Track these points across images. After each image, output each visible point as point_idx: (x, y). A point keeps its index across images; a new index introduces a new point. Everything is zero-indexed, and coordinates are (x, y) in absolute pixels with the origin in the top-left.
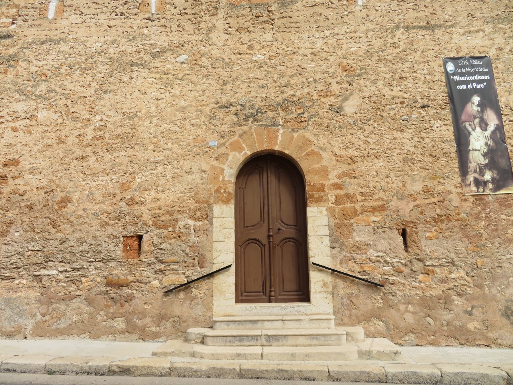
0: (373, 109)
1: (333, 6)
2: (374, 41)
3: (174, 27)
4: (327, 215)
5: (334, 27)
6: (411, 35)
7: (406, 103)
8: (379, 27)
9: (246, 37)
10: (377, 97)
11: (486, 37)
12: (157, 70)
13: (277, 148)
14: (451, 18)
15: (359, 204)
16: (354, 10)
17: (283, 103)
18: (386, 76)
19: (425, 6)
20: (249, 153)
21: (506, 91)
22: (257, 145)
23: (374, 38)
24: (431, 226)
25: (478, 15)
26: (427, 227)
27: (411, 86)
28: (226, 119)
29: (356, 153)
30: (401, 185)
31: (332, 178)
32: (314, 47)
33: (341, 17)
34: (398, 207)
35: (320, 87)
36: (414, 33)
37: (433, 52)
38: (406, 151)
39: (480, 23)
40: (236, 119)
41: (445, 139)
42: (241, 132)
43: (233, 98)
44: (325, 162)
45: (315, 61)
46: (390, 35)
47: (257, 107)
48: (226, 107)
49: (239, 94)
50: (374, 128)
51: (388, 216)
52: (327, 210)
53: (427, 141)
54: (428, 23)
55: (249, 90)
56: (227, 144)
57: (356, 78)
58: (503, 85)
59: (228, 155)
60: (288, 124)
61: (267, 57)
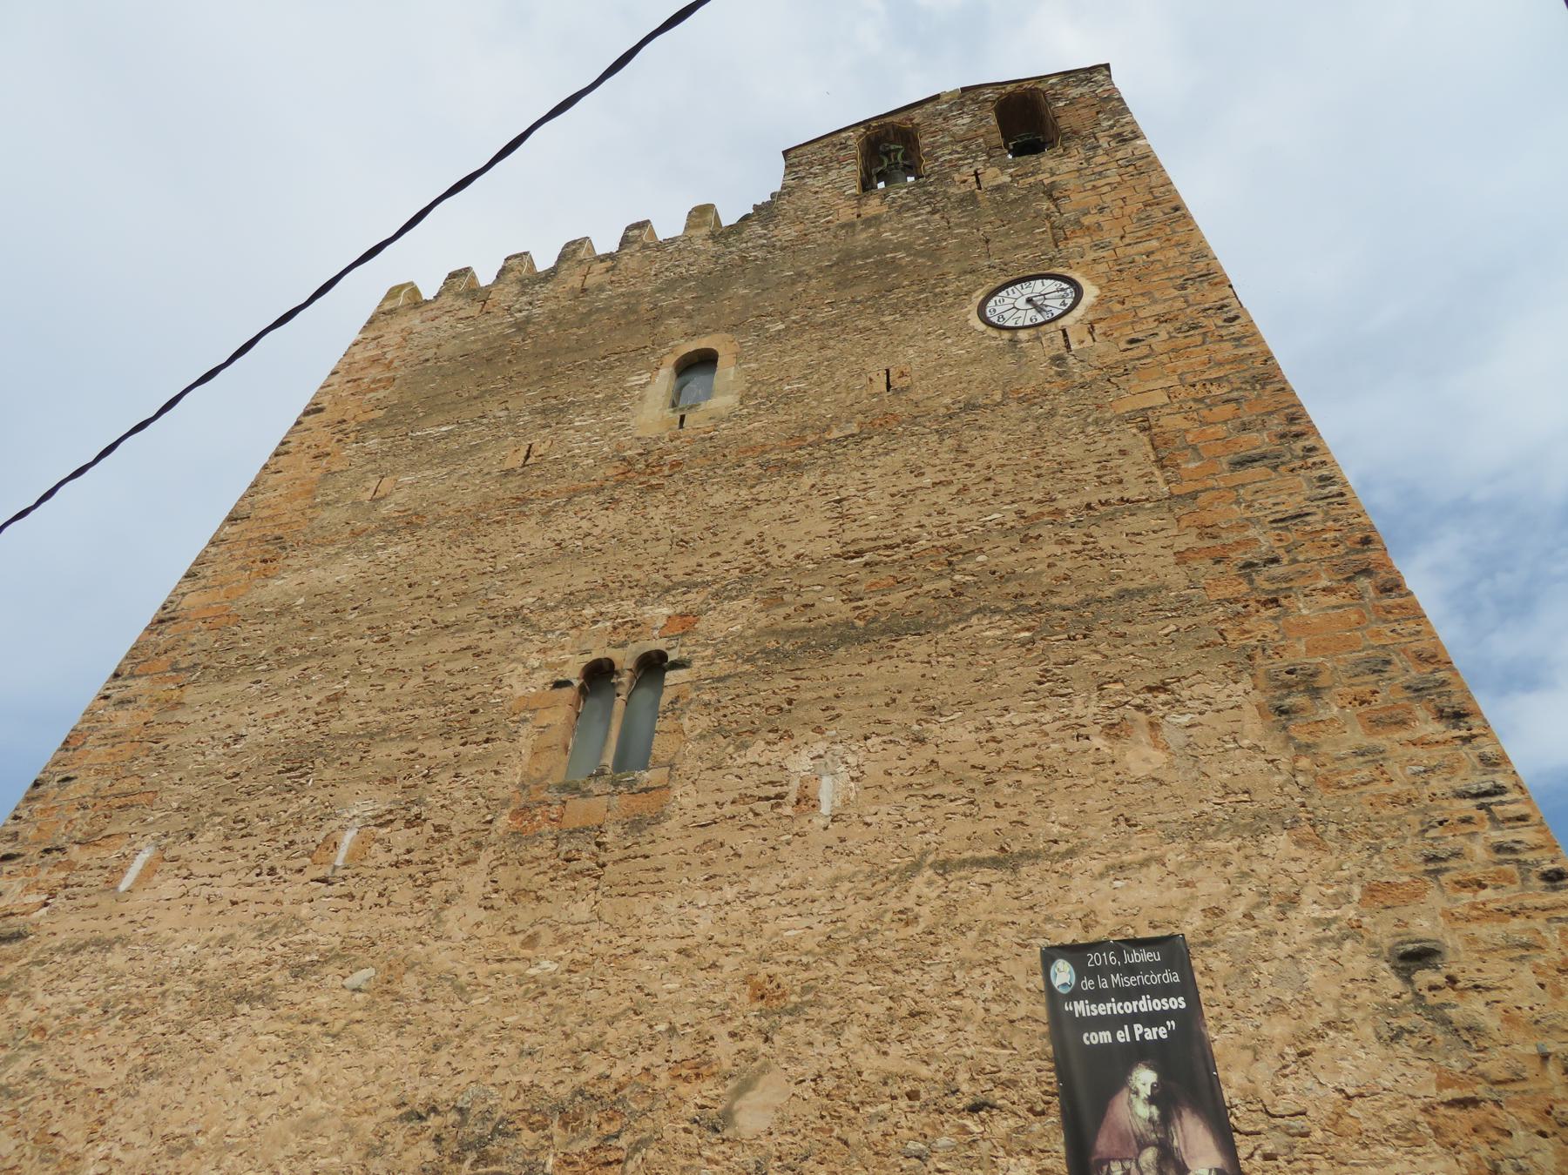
0: (822, 1117)
1: (758, 822)
2: (851, 908)
3: (372, 897)
6: (951, 886)
7: (924, 1096)
8: (866, 868)
9: (525, 914)
10: (839, 1077)
11: (1171, 879)
16: (807, 828)
19: (998, 805)
21: (1244, 1047)
23: (850, 900)
25: (1143, 817)
27: (942, 1038)
28: (406, 1156)
36: (961, 879)
37: (1013, 932)
39: (1150, 839)
43: (445, 1088)
47: (497, 1117)
48: (420, 1118)
54: (1002, 849)
57: (786, 1019)
61: (565, 964)
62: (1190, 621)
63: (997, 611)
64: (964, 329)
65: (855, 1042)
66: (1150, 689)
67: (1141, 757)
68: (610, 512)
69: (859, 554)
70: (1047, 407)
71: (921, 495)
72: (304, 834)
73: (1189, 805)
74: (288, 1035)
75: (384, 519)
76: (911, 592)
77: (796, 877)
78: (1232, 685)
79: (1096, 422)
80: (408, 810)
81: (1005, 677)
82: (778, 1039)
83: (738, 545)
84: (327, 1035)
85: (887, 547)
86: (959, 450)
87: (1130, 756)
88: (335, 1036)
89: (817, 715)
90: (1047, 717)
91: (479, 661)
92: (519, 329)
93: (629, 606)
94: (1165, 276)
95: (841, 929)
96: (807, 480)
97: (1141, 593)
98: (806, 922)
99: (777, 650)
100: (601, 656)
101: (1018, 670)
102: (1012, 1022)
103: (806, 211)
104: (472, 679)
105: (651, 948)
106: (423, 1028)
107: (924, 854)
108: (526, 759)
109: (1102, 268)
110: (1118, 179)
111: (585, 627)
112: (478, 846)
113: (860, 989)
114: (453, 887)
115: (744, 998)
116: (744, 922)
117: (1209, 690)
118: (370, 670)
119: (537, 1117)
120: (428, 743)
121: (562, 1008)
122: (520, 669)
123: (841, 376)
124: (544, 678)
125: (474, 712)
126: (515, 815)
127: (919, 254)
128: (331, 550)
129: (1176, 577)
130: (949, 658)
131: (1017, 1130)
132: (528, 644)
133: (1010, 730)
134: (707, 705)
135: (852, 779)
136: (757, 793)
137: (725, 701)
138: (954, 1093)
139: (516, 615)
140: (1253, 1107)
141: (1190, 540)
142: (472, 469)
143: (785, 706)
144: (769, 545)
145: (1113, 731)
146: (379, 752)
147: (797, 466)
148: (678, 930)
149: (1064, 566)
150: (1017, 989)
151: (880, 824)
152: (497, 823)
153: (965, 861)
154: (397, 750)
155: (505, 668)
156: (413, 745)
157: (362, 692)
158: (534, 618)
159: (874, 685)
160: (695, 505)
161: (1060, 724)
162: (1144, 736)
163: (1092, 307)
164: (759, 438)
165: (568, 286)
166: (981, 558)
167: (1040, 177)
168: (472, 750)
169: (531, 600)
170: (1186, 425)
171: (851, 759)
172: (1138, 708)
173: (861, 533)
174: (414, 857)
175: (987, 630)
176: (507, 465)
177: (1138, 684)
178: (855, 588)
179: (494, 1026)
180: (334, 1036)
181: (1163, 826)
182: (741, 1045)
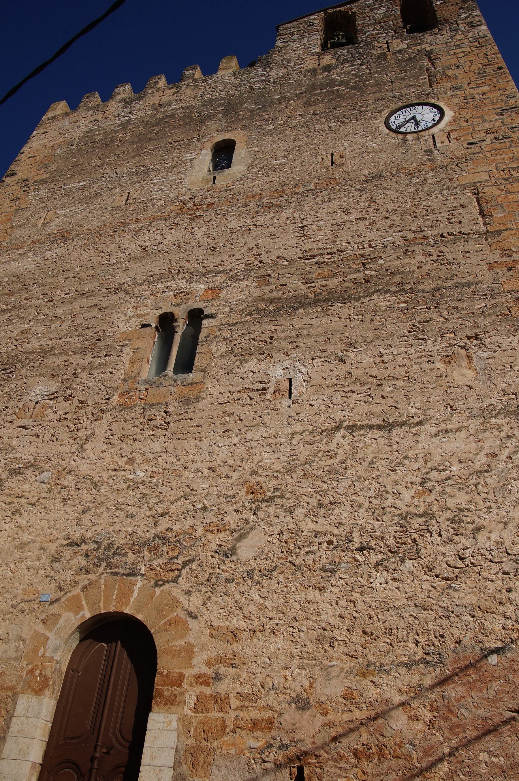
0: (282, 552)
1: (252, 402)
2: (301, 448)
3: (48, 436)
4: (178, 729)
5: (247, 431)
6: (355, 439)
7: (335, 543)
8: (310, 428)
9: (127, 447)
10: (292, 533)
11: (472, 438)
12: (11, 492)
13: (127, 610)
14: (419, 412)
15: (232, 714)
16: (279, 406)
17: (153, 540)
18: (310, 501)
19: (383, 397)
20: (88, 615)
21: (500, 522)
22: (101, 604)
23: (301, 445)
24: (347, 766)
25: (460, 405)
26: (340, 768)
27: (346, 516)
28: (72, 562)
29: (242, 624)
30: (307, 685)
31: (199, 666)
32: (214, 459)
33: (261, 417)
34: (294, 724)
35: (211, 517)
36: (361, 435)
37: (387, 463)
38: (323, 624)
39: (463, 418)
40: (84, 563)
41: (391, 605)
42: (86, 582)
43: (89, 532)
44: (191, 638)
45: (211, 478)
46: (325, 440)
47: (116, 547)
48: (77, 545)
49: (96, 526)
50: (278, 583)
51: (276, 740)
52: (178, 720)
53: (360, 608)
54: (384, 420)
55: (112, 521)
56: (63, 600)
57: (265, 504)
58: (495, 511)
59: (60, 615)
60: (152, 574)
61: (149, 473)
62: (493, 301)
63: (388, 291)
64: (375, 133)
65: (300, 517)
66: (469, 338)
67: (462, 374)
68: (173, 231)
69: (313, 257)
70: (422, 178)
71: (348, 225)
72: (12, 403)
73: (484, 400)
74: (10, 503)
75: (49, 235)
76: (341, 279)
77: (272, 432)
78: (512, 337)
79: (448, 188)
80: (65, 391)
81: (391, 328)
82: (261, 514)
83: (245, 250)
84: (29, 504)
85: (328, 254)
86: (371, 200)
87: (455, 373)
88: (33, 505)
89: (286, 345)
90: (413, 351)
91: (101, 313)
92: (123, 128)
93: (183, 283)
94: (492, 107)
95: (295, 460)
96: (284, 216)
97: (467, 284)
98: (277, 455)
99: (265, 309)
100: (168, 311)
101: (398, 324)
102: (383, 508)
103: (288, 61)
104: (97, 323)
105: (194, 466)
106: (77, 502)
107: (342, 422)
108: (127, 366)
109: (456, 101)
110: (469, 49)
111: (159, 295)
112: (102, 411)
113: (304, 490)
114: (89, 432)
115: (243, 493)
116: (243, 454)
117: (499, 339)
118: (43, 317)
119: (136, 547)
120: (75, 356)
121: (147, 495)
122: (123, 318)
123: (306, 156)
124: (136, 322)
125: (99, 340)
126: (121, 395)
127: (353, 88)
128: (21, 252)
129: (487, 277)
130: (360, 317)
131: (382, 560)
132: (127, 304)
133: (391, 357)
134: (225, 339)
135: (304, 381)
136: (252, 387)
137: (236, 337)
138: (350, 541)
139: (120, 288)
140: (501, 550)
141: (496, 256)
142: (97, 207)
143: (269, 340)
144: (262, 251)
145: (448, 359)
146: (49, 361)
147: (278, 206)
148: (208, 458)
149: (426, 268)
150: (387, 492)
151: (318, 406)
152: (112, 400)
153: (363, 426)
154: (58, 361)
155: (115, 316)
156: (67, 358)
157: (39, 328)
158: (130, 290)
159: (318, 330)
160: (221, 227)
161: (419, 354)
162: (464, 363)
163: (450, 123)
164: (257, 190)
165: (151, 103)
166: (381, 262)
167: (424, 46)
168: (98, 361)
169: (128, 279)
170: (498, 193)
171: (304, 370)
172: (462, 347)
173: (314, 246)
174: (69, 416)
175: (381, 301)
176: (116, 204)
177: (462, 334)
178: (309, 276)
179: (112, 503)
180: (33, 505)
181: (469, 411)
182: (241, 516)
